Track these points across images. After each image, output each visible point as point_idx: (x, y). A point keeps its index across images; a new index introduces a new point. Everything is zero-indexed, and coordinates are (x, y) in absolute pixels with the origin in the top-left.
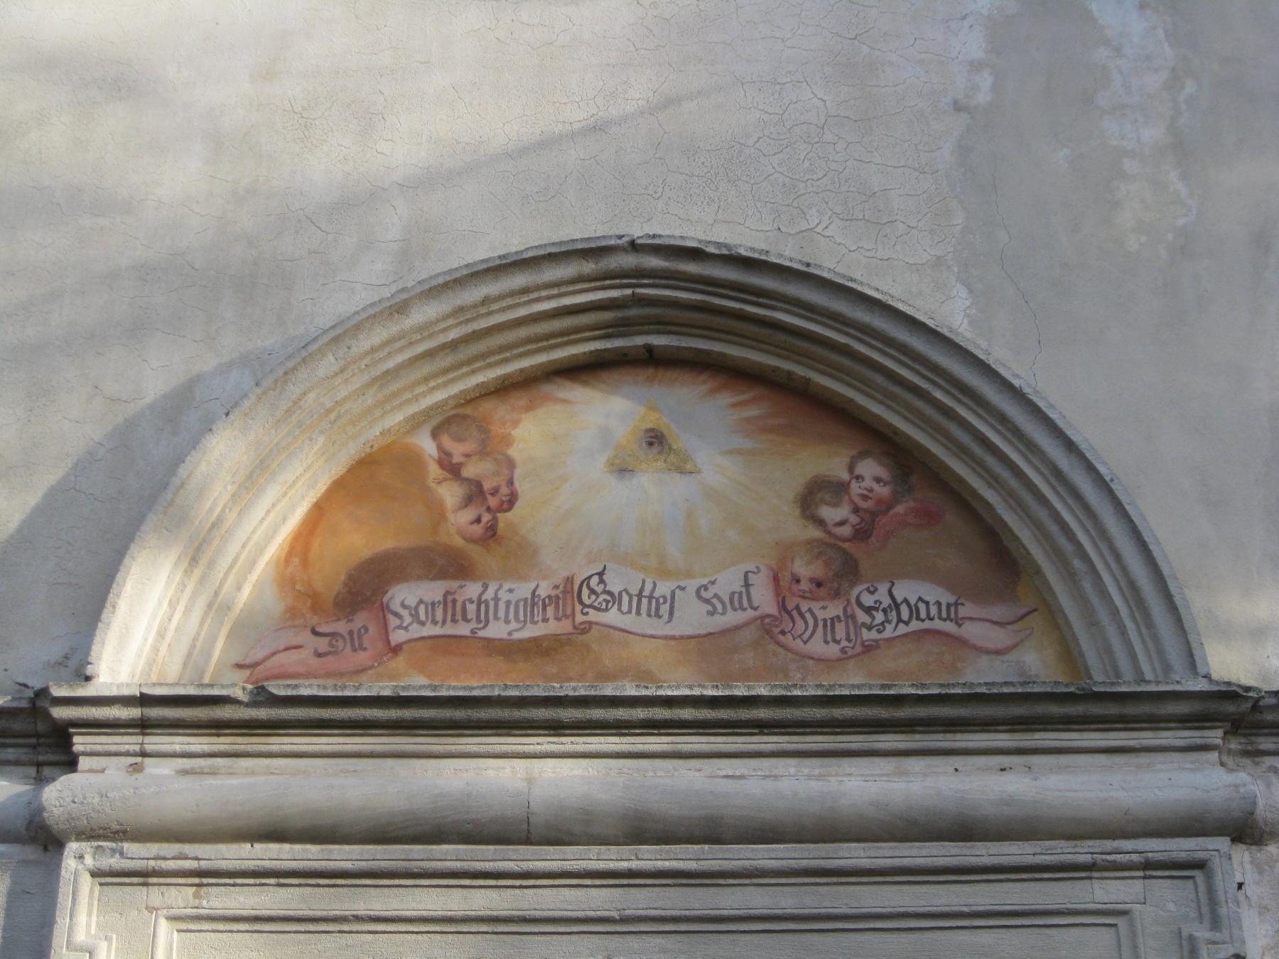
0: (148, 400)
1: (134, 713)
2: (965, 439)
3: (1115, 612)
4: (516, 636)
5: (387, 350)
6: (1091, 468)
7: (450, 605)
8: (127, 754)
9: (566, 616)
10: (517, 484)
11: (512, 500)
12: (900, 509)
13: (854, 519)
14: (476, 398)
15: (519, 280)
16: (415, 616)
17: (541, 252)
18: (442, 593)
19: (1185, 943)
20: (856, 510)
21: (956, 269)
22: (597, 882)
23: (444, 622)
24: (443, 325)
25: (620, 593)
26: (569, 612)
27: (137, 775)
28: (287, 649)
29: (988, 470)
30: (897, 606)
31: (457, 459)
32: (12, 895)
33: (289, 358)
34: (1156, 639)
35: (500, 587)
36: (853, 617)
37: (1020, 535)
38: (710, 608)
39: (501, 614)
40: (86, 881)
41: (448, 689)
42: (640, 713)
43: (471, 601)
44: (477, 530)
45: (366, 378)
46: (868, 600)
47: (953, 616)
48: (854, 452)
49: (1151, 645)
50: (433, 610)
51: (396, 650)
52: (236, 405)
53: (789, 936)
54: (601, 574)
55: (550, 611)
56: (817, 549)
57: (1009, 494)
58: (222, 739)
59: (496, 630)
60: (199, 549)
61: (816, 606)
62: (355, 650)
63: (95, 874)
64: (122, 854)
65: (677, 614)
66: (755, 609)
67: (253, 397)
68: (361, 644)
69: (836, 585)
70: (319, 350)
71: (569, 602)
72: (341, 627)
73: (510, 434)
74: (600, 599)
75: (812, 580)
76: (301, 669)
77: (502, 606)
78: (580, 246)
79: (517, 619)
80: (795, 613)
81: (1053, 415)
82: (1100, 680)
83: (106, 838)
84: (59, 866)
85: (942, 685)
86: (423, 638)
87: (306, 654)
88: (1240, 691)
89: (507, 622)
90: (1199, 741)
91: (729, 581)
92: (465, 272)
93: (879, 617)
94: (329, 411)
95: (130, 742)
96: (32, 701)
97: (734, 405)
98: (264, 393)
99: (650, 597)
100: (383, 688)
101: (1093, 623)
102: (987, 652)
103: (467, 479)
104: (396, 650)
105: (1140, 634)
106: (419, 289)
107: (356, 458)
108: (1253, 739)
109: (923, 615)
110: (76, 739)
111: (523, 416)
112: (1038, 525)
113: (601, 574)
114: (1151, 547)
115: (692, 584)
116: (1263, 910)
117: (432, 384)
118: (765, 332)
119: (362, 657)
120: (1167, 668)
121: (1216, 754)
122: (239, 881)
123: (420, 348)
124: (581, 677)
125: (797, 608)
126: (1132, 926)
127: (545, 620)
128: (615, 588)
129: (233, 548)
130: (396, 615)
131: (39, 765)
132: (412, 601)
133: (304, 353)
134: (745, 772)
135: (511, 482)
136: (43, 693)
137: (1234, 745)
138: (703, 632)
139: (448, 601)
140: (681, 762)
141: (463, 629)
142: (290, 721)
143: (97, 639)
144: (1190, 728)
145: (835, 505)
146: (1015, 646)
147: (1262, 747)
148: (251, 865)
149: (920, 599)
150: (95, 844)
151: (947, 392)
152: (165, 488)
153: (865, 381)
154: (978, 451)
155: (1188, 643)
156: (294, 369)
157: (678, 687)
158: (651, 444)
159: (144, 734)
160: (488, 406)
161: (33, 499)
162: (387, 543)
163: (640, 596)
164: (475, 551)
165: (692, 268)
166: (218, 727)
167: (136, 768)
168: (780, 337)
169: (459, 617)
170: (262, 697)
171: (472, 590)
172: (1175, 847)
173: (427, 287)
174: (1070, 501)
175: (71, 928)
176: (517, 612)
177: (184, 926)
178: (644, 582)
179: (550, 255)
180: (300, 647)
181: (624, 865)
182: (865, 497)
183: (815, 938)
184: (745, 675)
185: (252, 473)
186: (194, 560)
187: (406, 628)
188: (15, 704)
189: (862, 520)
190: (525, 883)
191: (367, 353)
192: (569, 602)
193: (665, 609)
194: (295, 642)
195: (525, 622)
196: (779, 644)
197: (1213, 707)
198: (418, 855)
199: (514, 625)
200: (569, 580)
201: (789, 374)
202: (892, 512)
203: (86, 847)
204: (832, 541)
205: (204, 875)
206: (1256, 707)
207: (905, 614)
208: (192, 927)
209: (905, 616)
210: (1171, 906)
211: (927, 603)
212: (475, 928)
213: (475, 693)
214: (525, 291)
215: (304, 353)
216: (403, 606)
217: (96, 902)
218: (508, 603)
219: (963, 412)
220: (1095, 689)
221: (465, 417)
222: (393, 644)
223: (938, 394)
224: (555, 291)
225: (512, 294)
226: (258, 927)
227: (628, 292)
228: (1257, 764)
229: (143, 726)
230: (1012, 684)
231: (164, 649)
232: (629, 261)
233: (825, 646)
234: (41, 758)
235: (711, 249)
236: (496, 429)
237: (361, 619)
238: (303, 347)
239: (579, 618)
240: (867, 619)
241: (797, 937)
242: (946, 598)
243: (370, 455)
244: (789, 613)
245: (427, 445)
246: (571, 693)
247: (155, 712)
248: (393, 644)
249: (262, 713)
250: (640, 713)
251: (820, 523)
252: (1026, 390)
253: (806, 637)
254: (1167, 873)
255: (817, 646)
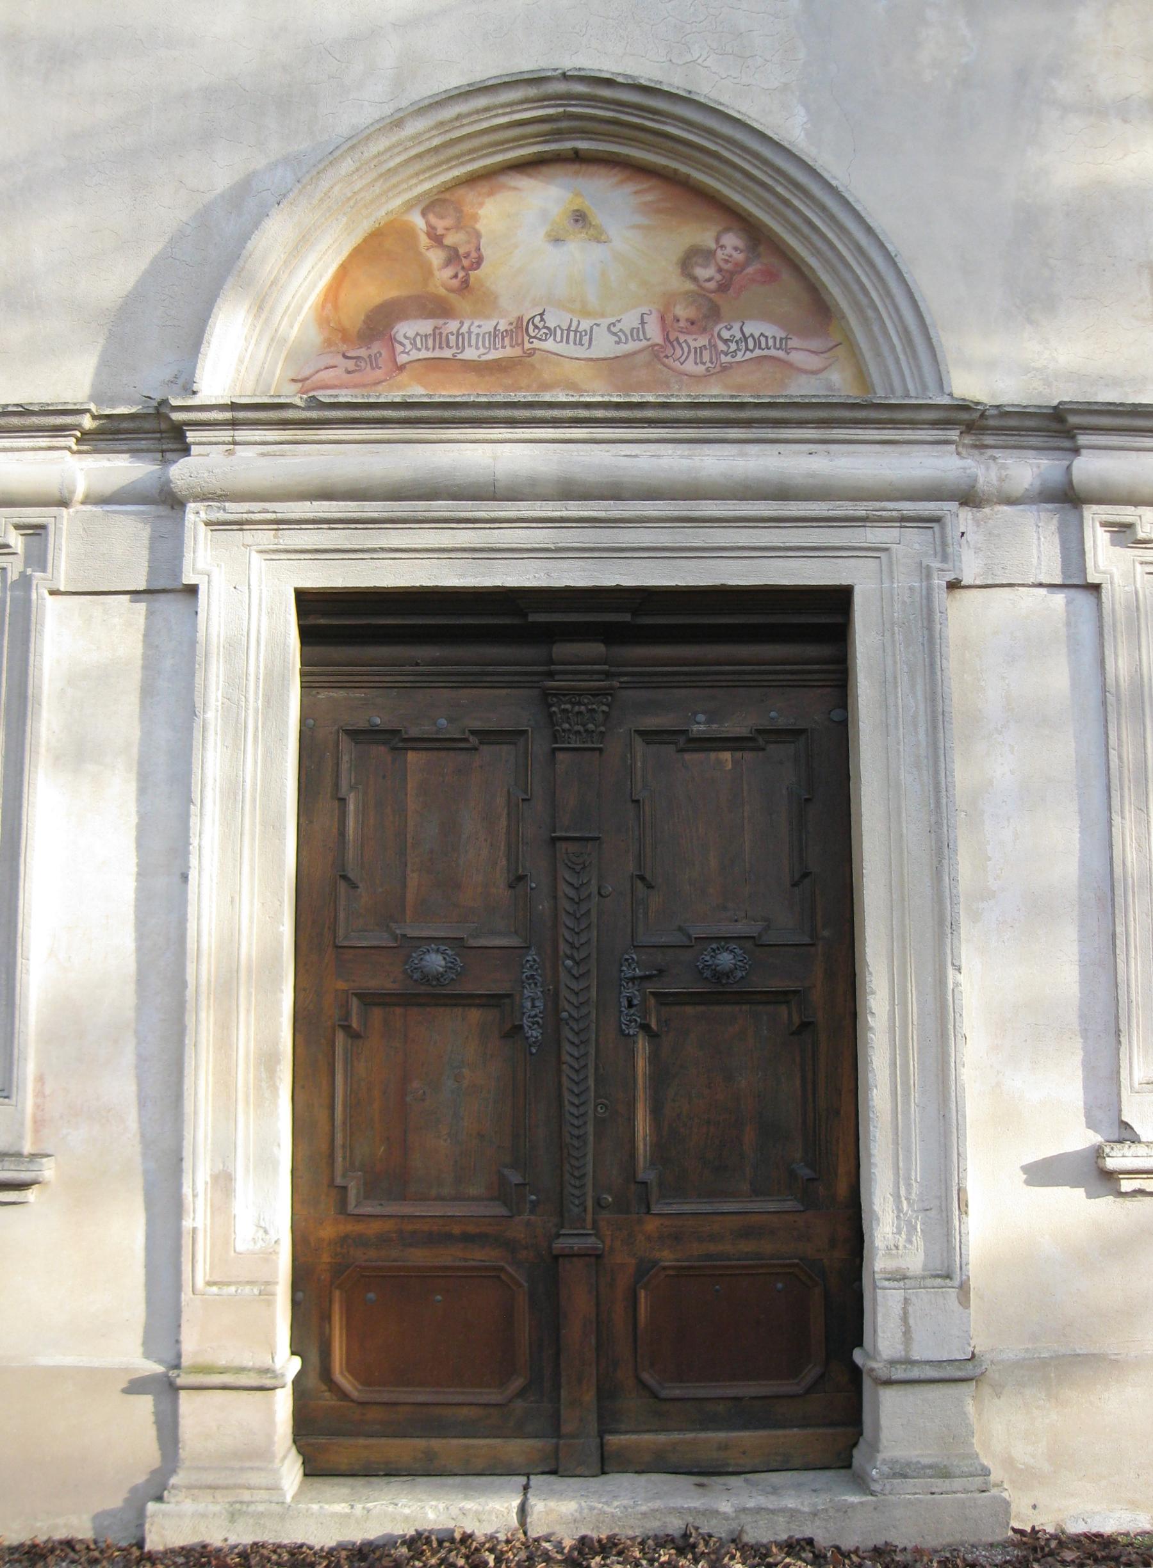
0: (219, 191)
1: (228, 415)
2: (798, 221)
3: (893, 348)
4: (484, 358)
5: (389, 154)
6: (882, 246)
7: (438, 337)
8: (224, 443)
9: (518, 345)
10: (482, 250)
11: (478, 263)
12: (750, 270)
13: (718, 277)
14: (453, 187)
15: (482, 102)
16: (414, 344)
17: (499, 81)
18: (432, 328)
19: (923, 570)
20: (720, 270)
21: (798, 93)
22: (540, 525)
23: (434, 349)
24: (428, 135)
25: (555, 328)
26: (520, 341)
27: (231, 458)
28: (327, 368)
29: (811, 243)
30: (746, 339)
31: (440, 232)
32: (153, 540)
33: (320, 161)
34: (919, 367)
35: (472, 323)
36: (715, 346)
37: (832, 291)
38: (617, 339)
39: (473, 342)
40: (202, 528)
41: (439, 397)
42: (568, 413)
43: (452, 334)
44: (455, 283)
45: (374, 174)
46: (726, 335)
47: (784, 347)
48: (720, 228)
49: (915, 372)
50: (426, 341)
51: (401, 368)
52: (285, 196)
53: (667, 561)
54: (541, 315)
55: (507, 341)
56: (691, 298)
57: (826, 262)
58: (287, 432)
59: (470, 354)
60: (263, 301)
61: (690, 339)
62: (373, 368)
63: (207, 524)
64: (224, 510)
65: (594, 343)
66: (648, 340)
67: (296, 191)
68: (377, 365)
69: (704, 324)
70: (342, 155)
71: (520, 333)
72: (362, 352)
73: (477, 213)
74: (541, 332)
75: (687, 320)
76: (336, 382)
77: (473, 337)
78: (526, 76)
79: (484, 345)
80: (675, 343)
81: (858, 207)
82: (880, 395)
83: (213, 500)
84: (183, 519)
85: (771, 396)
86: (419, 360)
87: (339, 371)
88: (972, 405)
89: (477, 348)
90: (943, 438)
91: (630, 320)
92: (444, 96)
93: (733, 347)
94: (349, 199)
95: (225, 435)
96: (157, 408)
97: (636, 193)
98: (304, 187)
99: (576, 331)
100: (395, 396)
101: (878, 355)
102: (806, 372)
103: (448, 247)
104: (401, 368)
105: (909, 363)
106: (411, 109)
107: (369, 231)
108: (981, 437)
109: (763, 346)
110: (188, 434)
111: (487, 200)
112: (845, 285)
113: (541, 315)
114: (920, 304)
115: (605, 322)
116: (978, 550)
117: (421, 177)
118: (659, 140)
119: (379, 374)
120: (925, 388)
121: (954, 446)
122: (303, 526)
123: (413, 152)
124: (528, 388)
125: (677, 339)
126: (890, 558)
127: (503, 347)
128: (551, 324)
129: (286, 298)
130: (401, 344)
131: (163, 451)
132: (411, 334)
133: (331, 158)
134: (638, 452)
135: (478, 249)
136: (164, 402)
137: (968, 440)
138: (612, 356)
139: (436, 333)
140: (595, 445)
141: (447, 353)
142: (332, 419)
143: (199, 365)
144: (937, 429)
145: (705, 266)
146: (825, 368)
147: (986, 443)
148: (311, 516)
149: (762, 334)
150: (207, 504)
151: (786, 188)
152: (239, 258)
153: (729, 178)
154: (806, 230)
155: (939, 371)
156: (324, 169)
157: (594, 396)
158: (577, 221)
159: (234, 430)
160: (461, 192)
161: (143, 265)
162: (393, 293)
163: (569, 330)
164: (452, 297)
165: (606, 93)
166: (284, 424)
167: (230, 453)
168: (670, 144)
169: (444, 345)
170: (314, 403)
171: (453, 325)
172: (921, 508)
173: (416, 107)
174: (867, 269)
175: (194, 560)
176: (484, 342)
177: (269, 557)
178: (571, 320)
179: (505, 83)
180: (335, 367)
181: (557, 514)
182: (726, 261)
183: (683, 562)
184: (639, 387)
185: (297, 246)
186: (260, 308)
187: (408, 353)
188: (145, 411)
189: (724, 277)
190: (492, 526)
191: (375, 157)
192: (520, 333)
193: (586, 339)
194: (332, 362)
195: (490, 348)
196: (665, 365)
197: (954, 415)
198: (420, 507)
199: (482, 350)
200: (520, 319)
201: (675, 171)
202: (746, 272)
203: (200, 506)
204: (703, 293)
205: (280, 523)
206: (983, 415)
207: (751, 345)
208: (274, 557)
209: (751, 346)
210: (917, 546)
211: (767, 337)
212: (459, 555)
213: (458, 400)
214: (486, 109)
215: (331, 158)
216: (406, 337)
217: (209, 542)
218: (478, 335)
219: (796, 202)
220: (875, 401)
221: (444, 201)
222: (399, 364)
223: (779, 189)
224: (508, 110)
225: (478, 112)
226: (317, 556)
227: (561, 110)
228: (982, 454)
229: (234, 424)
230: (818, 396)
231: (243, 370)
232: (561, 87)
233: (695, 367)
234: (164, 447)
235: (620, 80)
236: (467, 209)
237: (376, 347)
238: (330, 153)
239: (527, 346)
240: (724, 348)
241: (672, 561)
242: (780, 334)
243: (378, 229)
244: (671, 343)
245: (418, 221)
246: (523, 400)
247: (241, 415)
248: (399, 364)
249: (314, 414)
250: (568, 413)
251: (695, 279)
252: (841, 188)
253: (682, 360)
254: (915, 525)
255: (690, 366)
